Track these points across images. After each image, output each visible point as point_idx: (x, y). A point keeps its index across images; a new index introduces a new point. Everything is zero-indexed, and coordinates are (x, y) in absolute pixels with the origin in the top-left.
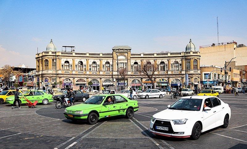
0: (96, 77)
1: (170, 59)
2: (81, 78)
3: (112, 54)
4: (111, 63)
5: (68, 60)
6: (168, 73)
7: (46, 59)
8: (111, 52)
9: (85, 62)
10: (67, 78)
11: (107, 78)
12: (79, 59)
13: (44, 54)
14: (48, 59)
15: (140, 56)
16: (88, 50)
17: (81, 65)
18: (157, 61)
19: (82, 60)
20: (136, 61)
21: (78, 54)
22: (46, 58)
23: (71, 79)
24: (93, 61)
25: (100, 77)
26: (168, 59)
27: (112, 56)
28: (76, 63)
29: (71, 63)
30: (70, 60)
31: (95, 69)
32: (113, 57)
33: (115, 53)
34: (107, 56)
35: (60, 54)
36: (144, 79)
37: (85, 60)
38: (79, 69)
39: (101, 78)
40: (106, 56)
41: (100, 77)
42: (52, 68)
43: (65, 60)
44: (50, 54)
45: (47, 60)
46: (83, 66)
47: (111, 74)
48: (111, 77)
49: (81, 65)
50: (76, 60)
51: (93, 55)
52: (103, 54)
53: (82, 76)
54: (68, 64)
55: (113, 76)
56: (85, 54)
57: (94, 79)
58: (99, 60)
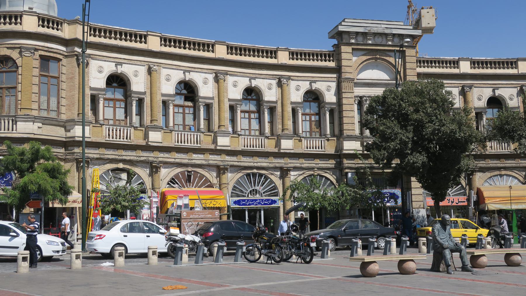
0: (263, 162)
2: (190, 169)
4: (330, 97)
5: (127, 69)
6: (280, 149)
9: (206, 89)
10: (121, 166)
11: (312, 169)
12: (178, 68)
15: (455, 71)
19: (261, 84)
21: (241, 50)
23: (143, 173)
25: (214, 159)
27: (332, 64)
31: (255, 125)
32: (338, 70)
33: (349, 49)
34: (123, 43)
37: (211, 77)
38: (179, 119)
39: (284, 172)
41: (214, 159)
42: (35, 106)
47: (330, 148)
48: (331, 164)
49: (187, 99)
50: (164, 72)
53: (198, 159)
55: (345, 161)
57: (254, 175)
58: (274, 82)
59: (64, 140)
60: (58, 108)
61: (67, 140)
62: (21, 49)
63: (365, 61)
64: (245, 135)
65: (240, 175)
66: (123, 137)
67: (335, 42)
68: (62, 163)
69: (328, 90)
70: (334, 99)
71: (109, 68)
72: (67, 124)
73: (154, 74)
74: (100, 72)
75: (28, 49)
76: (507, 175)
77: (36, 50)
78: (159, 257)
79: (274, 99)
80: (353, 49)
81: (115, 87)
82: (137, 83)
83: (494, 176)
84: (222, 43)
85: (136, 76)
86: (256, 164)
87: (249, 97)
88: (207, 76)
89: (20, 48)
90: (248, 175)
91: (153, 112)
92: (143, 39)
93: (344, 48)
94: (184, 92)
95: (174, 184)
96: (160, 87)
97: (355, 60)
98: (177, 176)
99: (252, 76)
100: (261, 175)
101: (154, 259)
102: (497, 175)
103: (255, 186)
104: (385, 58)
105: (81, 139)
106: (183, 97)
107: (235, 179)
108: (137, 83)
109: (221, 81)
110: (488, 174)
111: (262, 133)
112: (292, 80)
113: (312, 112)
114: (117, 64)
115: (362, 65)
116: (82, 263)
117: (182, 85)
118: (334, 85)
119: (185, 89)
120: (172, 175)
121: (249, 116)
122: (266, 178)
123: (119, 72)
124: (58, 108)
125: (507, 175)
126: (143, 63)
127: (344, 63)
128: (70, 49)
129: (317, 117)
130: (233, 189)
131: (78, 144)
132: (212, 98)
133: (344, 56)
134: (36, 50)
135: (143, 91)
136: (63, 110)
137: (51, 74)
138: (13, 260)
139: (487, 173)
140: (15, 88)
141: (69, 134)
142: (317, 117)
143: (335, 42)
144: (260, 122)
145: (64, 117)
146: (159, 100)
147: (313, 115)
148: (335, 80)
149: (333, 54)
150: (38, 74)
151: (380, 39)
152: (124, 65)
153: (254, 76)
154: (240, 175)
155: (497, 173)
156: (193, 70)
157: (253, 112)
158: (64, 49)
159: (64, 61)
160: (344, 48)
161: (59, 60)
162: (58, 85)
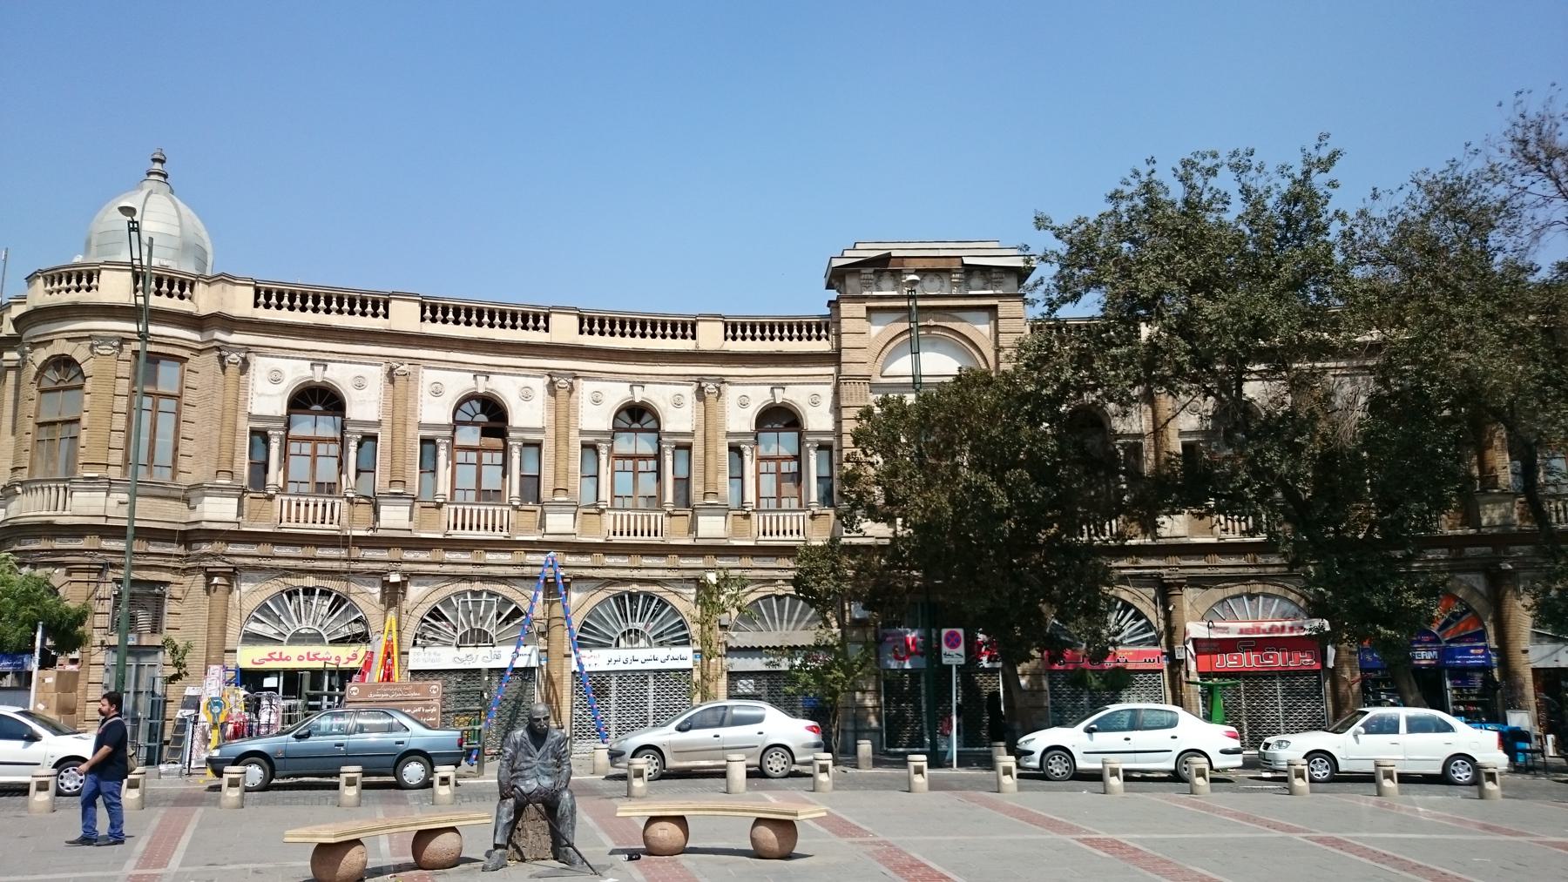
0: (654, 566)
1: (721, 380)
3: (827, 325)
5: (338, 375)
7: (61, 348)
8: (815, 302)
13: (40, 296)
14: (79, 353)
15: (378, 324)
16: (570, 278)
17: (486, 432)
18: (424, 390)
19: (506, 388)
20: (639, 396)
22: (61, 340)
24: (617, 394)
26: (700, 379)
27: (824, 346)
28: (733, 427)
29: (364, 404)
30: (363, 387)
32: (834, 358)
33: (859, 309)
35: (240, 302)
36: (1190, 594)
37: (539, 385)
38: (467, 476)
40: (763, 338)
42: (116, 457)
43: (297, 372)
44: (115, 288)
45: (64, 363)
46: (505, 451)
50: (428, 377)
51: (618, 333)
52: (734, 329)
54: (327, 427)
56: (537, 319)
57: (633, 597)
58: (689, 391)
59: (183, 528)
60: (175, 460)
61: (190, 527)
62: (89, 337)
63: (901, 334)
64: (624, 509)
65: (602, 595)
66: (324, 518)
67: (833, 295)
68: (58, 576)
69: (814, 404)
70: (827, 423)
71: (760, 397)
72: (189, 494)
73: (399, 381)
74: (276, 381)
75: (105, 340)
76: (1267, 596)
77: (124, 341)
78: (1126, 779)
79: (687, 428)
80: (868, 309)
81: (317, 413)
82: (363, 402)
83: (1232, 598)
84: (405, 296)
85: (360, 387)
86: (636, 574)
87: (636, 426)
88: (531, 382)
89: (89, 338)
90: (619, 598)
91: (396, 458)
92: (381, 309)
93: (846, 309)
94: (483, 418)
95: (437, 620)
96: (415, 410)
97: (879, 331)
98: (446, 602)
99: (635, 378)
100: (649, 597)
101: (1115, 782)
102: (1239, 596)
103: (300, 621)
104: (948, 325)
105: (125, 523)
106: (478, 429)
107: (587, 608)
108: (363, 402)
109: (711, 399)
110: (1217, 593)
111: (656, 501)
112: (730, 383)
113: (784, 452)
114: (633, 385)
115: (893, 345)
116: (359, 795)
117: (624, 415)
118: (826, 392)
119: (483, 412)
120: (434, 600)
121: (480, 458)
122: (663, 603)
123: (318, 380)
124: (175, 460)
125: (1267, 596)
126: (538, 372)
127: (846, 341)
128: (207, 336)
129: (794, 465)
130: (581, 630)
131: (212, 535)
132: (542, 430)
133: (846, 325)
134: (124, 341)
135: (375, 418)
136: (184, 464)
137: (161, 390)
138: (22, 790)
139: (1212, 591)
140: (77, 421)
141: (193, 517)
142: (794, 465)
143: (833, 295)
144: (658, 478)
145: (185, 480)
146: (415, 435)
147: (785, 459)
148: (830, 380)
149: (827, 325)
150: (126, 391)
151: (937, 283)
152: (330, 365)
153: (640, 379)
154: (602, 595)
155: (1236, 589)
156: (496, 370)
157: (645, 458)
158: (195, 336)
159: (195, 362)
160: (846, 309)
161: (183, 360)
162: (178, 413)
